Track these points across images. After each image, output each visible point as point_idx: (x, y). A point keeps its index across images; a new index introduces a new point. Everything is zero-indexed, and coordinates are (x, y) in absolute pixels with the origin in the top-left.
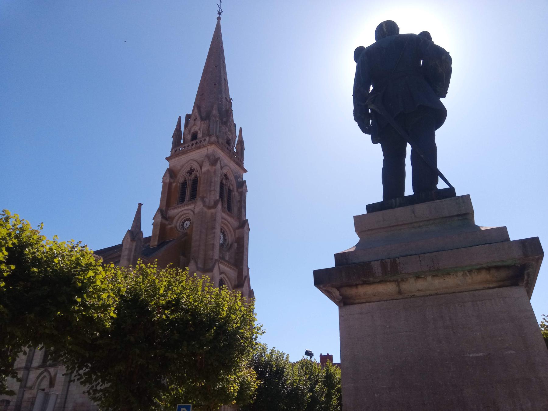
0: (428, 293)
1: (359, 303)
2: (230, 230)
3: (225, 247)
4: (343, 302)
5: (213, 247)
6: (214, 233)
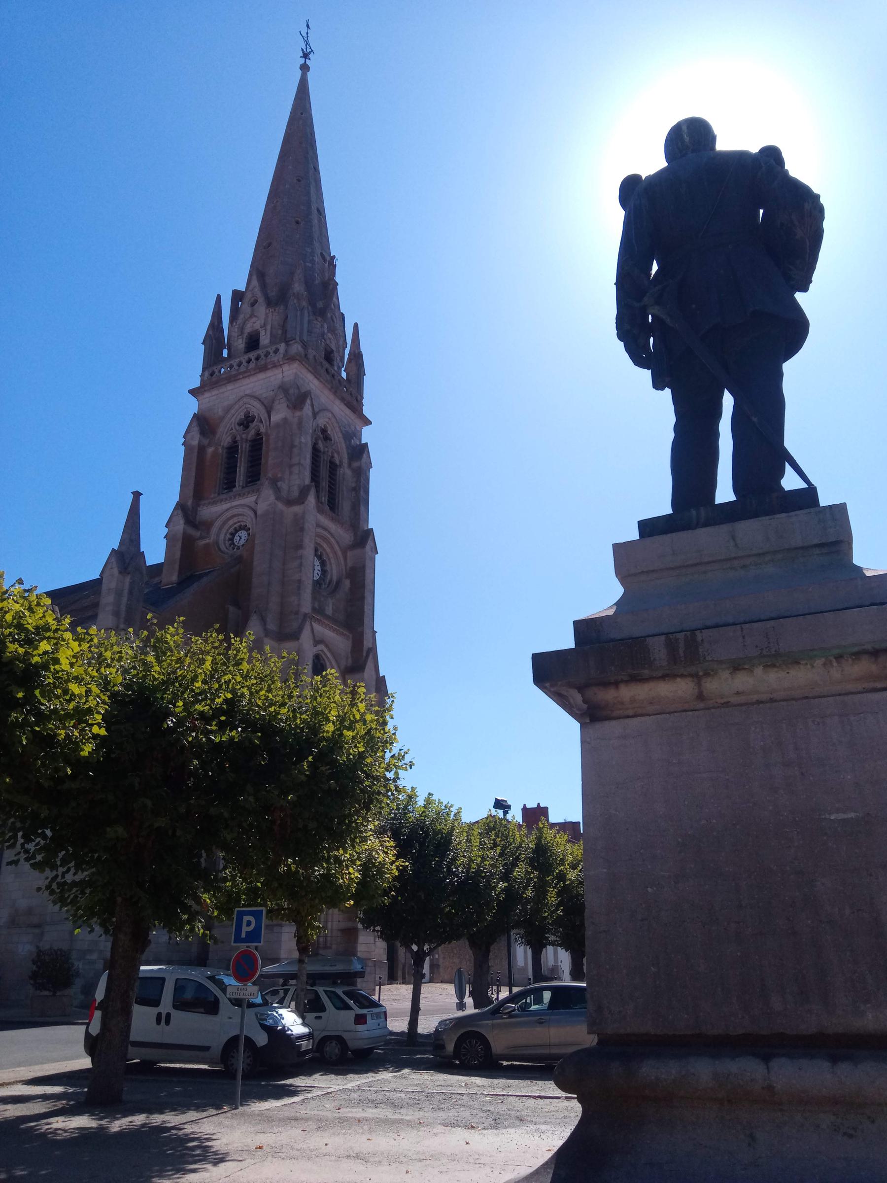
0: (755, 697)
1: (619, 718)
2: (335, 553)
3: (323, 586)
4: (590, 715)
5: (299, 588)
6: (301, 557)
